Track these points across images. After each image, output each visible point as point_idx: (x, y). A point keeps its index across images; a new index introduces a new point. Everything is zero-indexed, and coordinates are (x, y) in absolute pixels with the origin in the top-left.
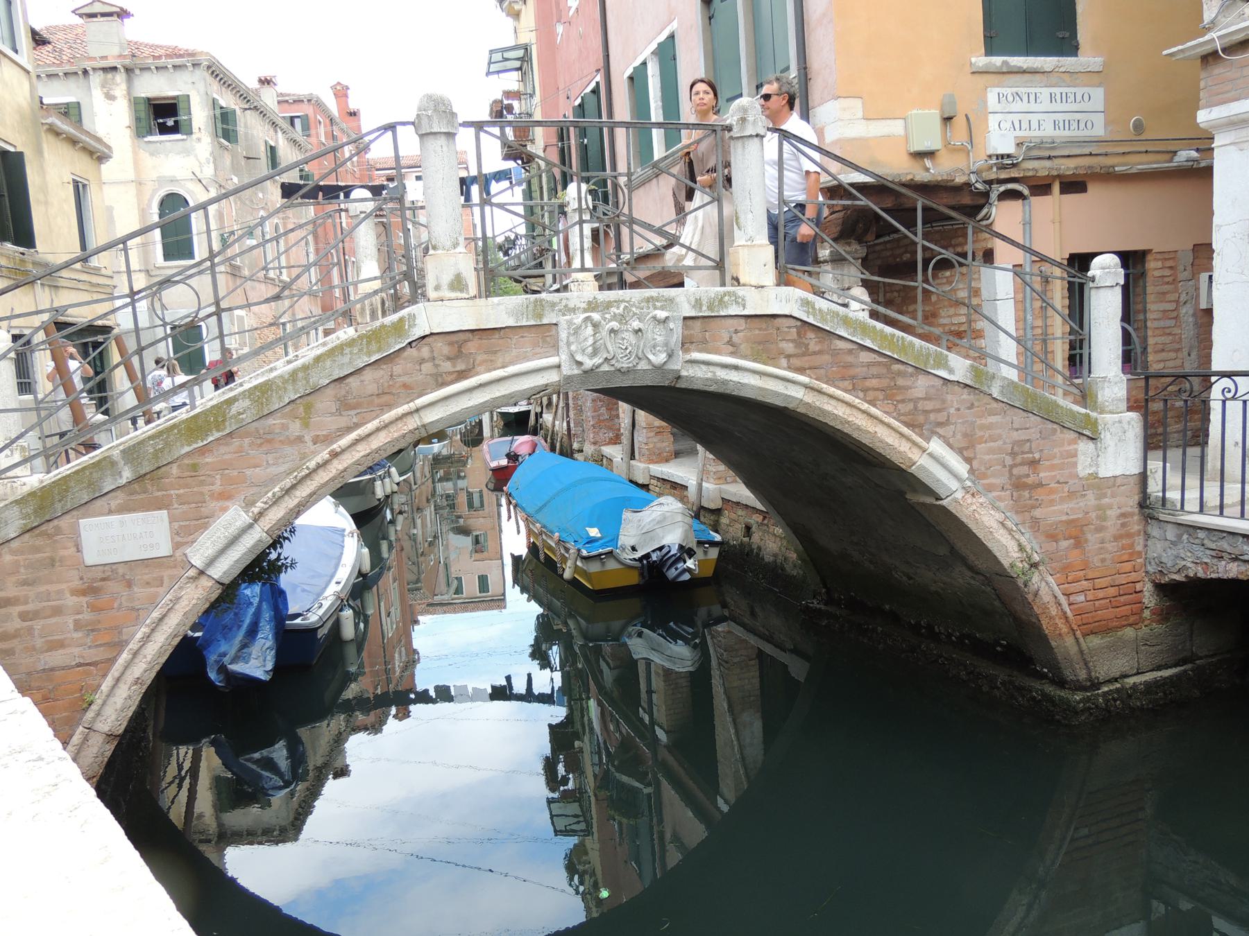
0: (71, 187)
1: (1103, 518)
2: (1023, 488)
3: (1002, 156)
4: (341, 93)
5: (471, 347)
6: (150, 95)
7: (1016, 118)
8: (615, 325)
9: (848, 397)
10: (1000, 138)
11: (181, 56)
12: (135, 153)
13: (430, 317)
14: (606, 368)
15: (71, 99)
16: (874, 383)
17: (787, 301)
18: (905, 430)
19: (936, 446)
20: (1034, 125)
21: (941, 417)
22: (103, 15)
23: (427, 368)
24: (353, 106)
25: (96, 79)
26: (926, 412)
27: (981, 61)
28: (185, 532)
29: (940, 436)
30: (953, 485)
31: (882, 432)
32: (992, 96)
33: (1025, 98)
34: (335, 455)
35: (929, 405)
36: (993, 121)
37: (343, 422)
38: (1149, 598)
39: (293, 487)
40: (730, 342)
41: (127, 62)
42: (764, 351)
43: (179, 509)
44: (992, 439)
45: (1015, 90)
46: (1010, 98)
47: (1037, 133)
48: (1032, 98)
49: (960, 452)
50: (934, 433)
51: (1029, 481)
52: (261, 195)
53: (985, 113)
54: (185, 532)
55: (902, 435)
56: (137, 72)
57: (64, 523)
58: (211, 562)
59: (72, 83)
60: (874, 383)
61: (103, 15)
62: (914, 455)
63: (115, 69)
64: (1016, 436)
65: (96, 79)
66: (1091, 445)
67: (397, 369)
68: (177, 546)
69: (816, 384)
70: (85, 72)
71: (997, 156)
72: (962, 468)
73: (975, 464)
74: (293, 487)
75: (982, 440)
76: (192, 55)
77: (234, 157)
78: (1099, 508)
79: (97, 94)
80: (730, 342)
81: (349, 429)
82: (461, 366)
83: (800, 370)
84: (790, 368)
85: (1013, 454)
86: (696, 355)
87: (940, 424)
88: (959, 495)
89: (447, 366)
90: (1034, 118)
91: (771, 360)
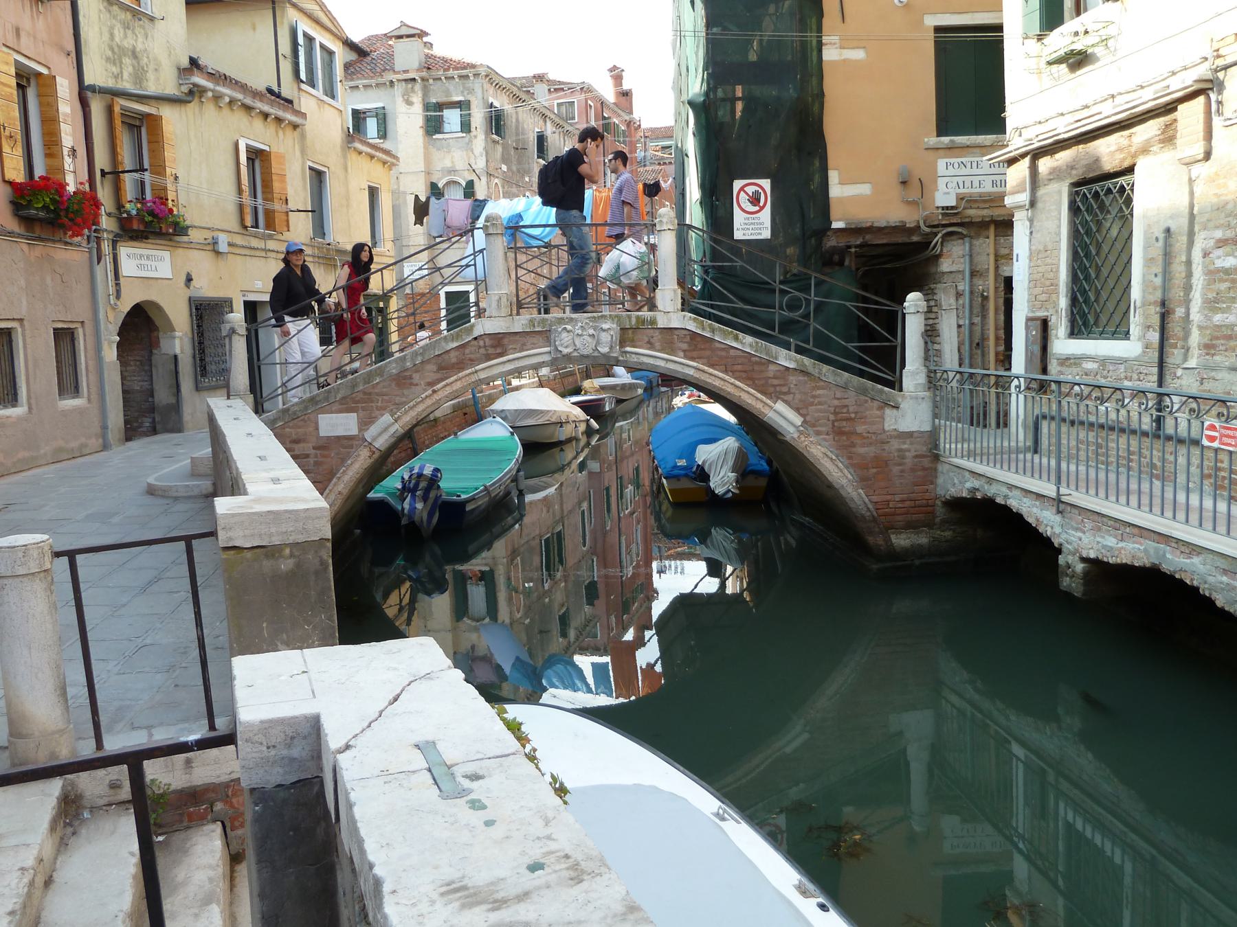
0: (367, 192)
1: (903, 457)
2: (842, 432)
3: (947, 208)
4: (617, 75)
5: (506, 341)
6: (421, 132)
7: (960, 180)
8: (580, 332)
9: (721, 375)
10: (945, 197)
11: (465, 68)
12: (426, 148)
13: (482, 327)
14: (575, 354)
15: (380, 105)
16: (739, 367)
17: (687, 322)
18: (759, 395)
19: (780, 406)
20: (976, 184)
21: (785, 389)
22: (408, 36)
23: (482, 351)
24: (626, 87)
25: (399, 89)
26: (775, 386)
27: (933, 140)
28: (365, 424)
29: (784, 401)
30: (791, 429)
31: (745, 397)
32: (941, 163)
33: (969, 165)
34: (434, 392)
35: (776, 382)
36: (941, 183)
37: (439, 376)
38: (940, 511)
39: (415, 406)
40: (649, 342)
41: (424, 74)
42: (669, 348)
43: (361, 413)
44: (820, 403)
45: (960, 160)
46: (956, 166)
47: (978, 190)
48: (975, 165)
49: (797, 410)
50: (778, 398)
51: (847, 429)
52: (527, 179)
53: (935, 177)
54: (365, 424)
55: (757, 399)
56: (431, 81)
57: (312, 416)
58: (375, 439)
59: (381, 92)
60: (739, 367)
61: (408, 36)
62: (766, 410)
63: (414, 79)
64: (836, 402)
65: (399, 89)
66: (895, 411)
67: (467, 351)
68: (360, 430)
69: (701, 366)
70: (392, 82)
71: (943, 208)
72: (798, 420)
73: (808, 418)
74: (415, 406)
75: (812, 404)
76: (473, 66)
77: (505, 147)
78: (900, 450)
79: (400, 100)
80: (649, 342)
81: (442, 380)
82: (499, 350)
83: (692, 359)
84: (686, 357)
85: (835, 413)
86: (628, 349)
87: (785, 393)
88: (796, 436)
89: (491, 351)
90: (976, 180)
91: (672, 352)
